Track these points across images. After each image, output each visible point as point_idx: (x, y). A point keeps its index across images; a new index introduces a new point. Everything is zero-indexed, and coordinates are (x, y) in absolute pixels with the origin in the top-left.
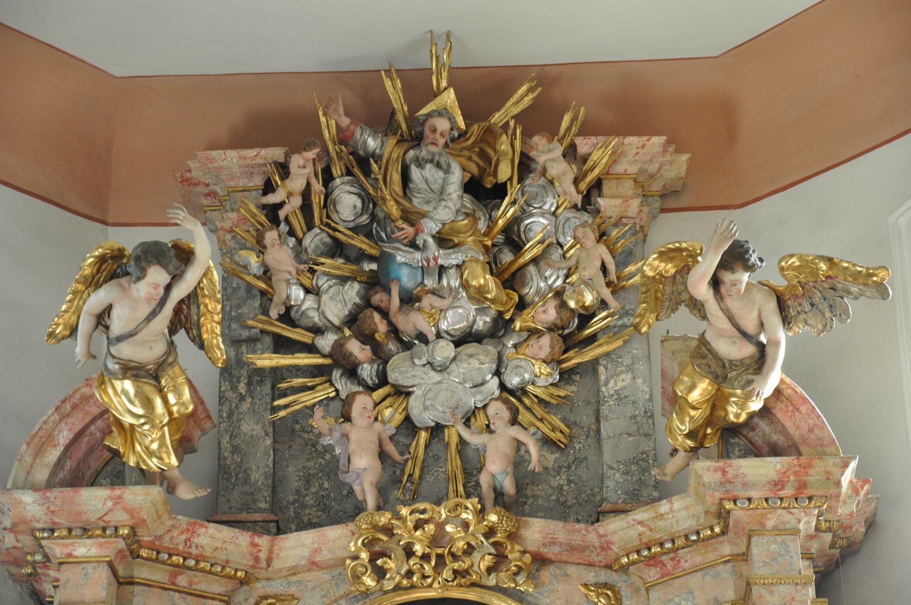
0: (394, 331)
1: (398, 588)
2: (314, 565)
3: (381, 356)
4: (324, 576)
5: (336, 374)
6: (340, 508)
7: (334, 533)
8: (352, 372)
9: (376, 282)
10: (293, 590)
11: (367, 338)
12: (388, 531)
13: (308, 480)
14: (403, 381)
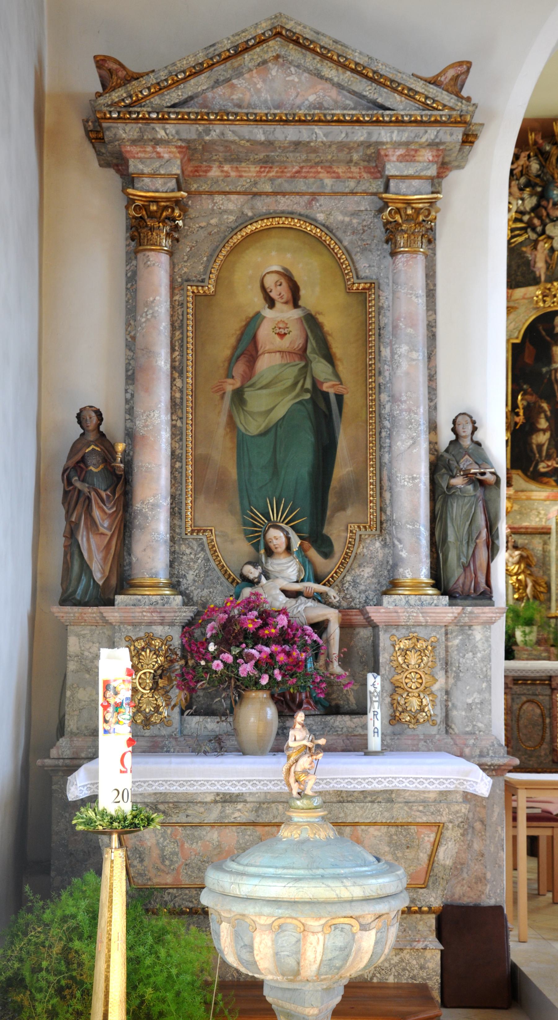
0: (548, 215)
1: (550, 306)
2: (524, 298)
3: (544, 225)
4: (526, 301)
5: (529, 230)
6: (535, 281)
7: (531, 289)
8: (534, 229)
9: (543, 196)
10: (516, 305)
11: (540, 217)
12: (549, 289)
13: (519, 267)
14: (551, 234)
